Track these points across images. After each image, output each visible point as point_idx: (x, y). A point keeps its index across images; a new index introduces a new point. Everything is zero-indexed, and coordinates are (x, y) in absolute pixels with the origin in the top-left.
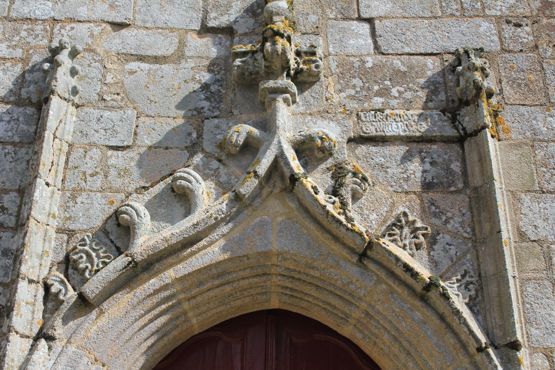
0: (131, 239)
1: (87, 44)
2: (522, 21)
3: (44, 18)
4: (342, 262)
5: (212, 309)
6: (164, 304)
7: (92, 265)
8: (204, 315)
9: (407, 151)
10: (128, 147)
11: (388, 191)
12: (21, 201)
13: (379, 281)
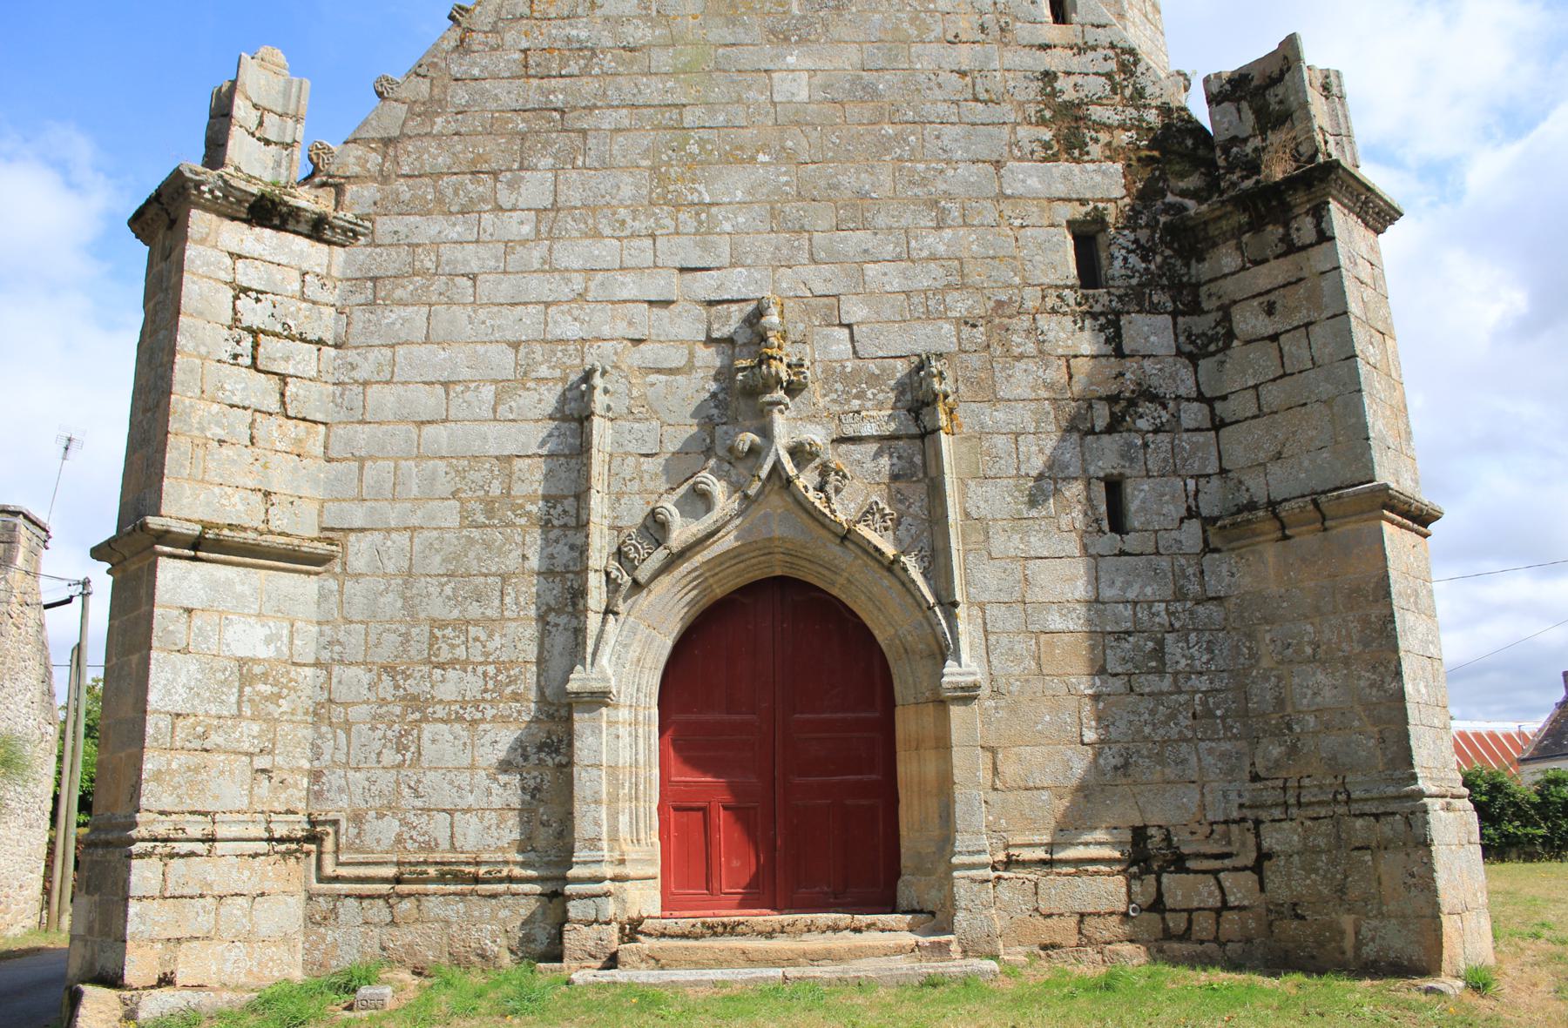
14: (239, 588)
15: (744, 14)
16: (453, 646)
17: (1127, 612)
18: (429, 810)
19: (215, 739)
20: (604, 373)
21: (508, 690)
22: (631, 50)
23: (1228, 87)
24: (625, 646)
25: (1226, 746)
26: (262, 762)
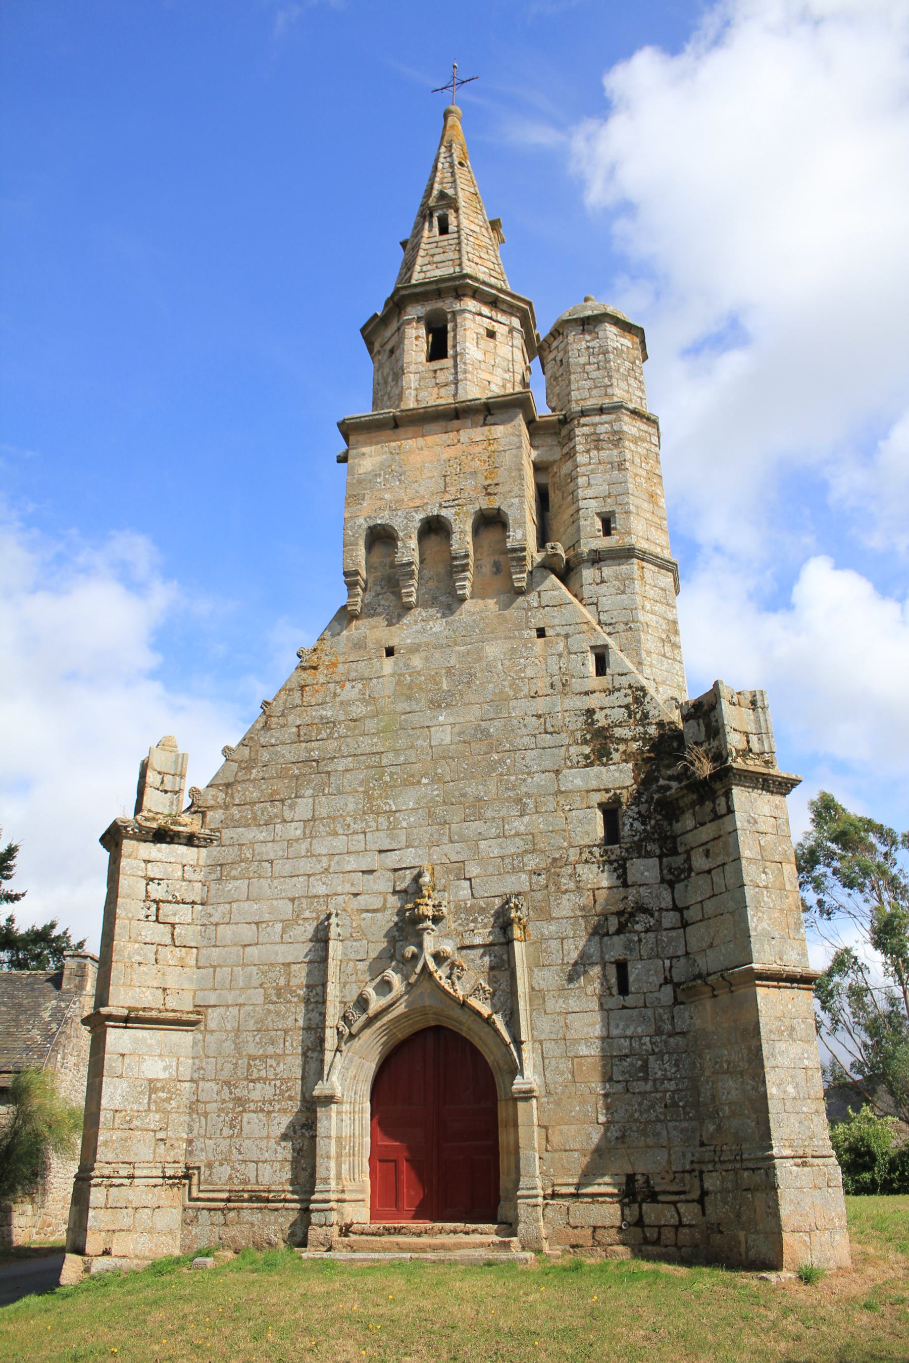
14: (149, 1041)
15: (416, 692)
16: (259, 1070)
17: (626, 1043)
18: (246, 1161)
19: (136, 1123)
20: (337, 915)
21: (287, 1094)
22: (355, 721)
23: (692, 710)
24: (347, 1069)
25: (685, 1124)
26: (160, 1135)
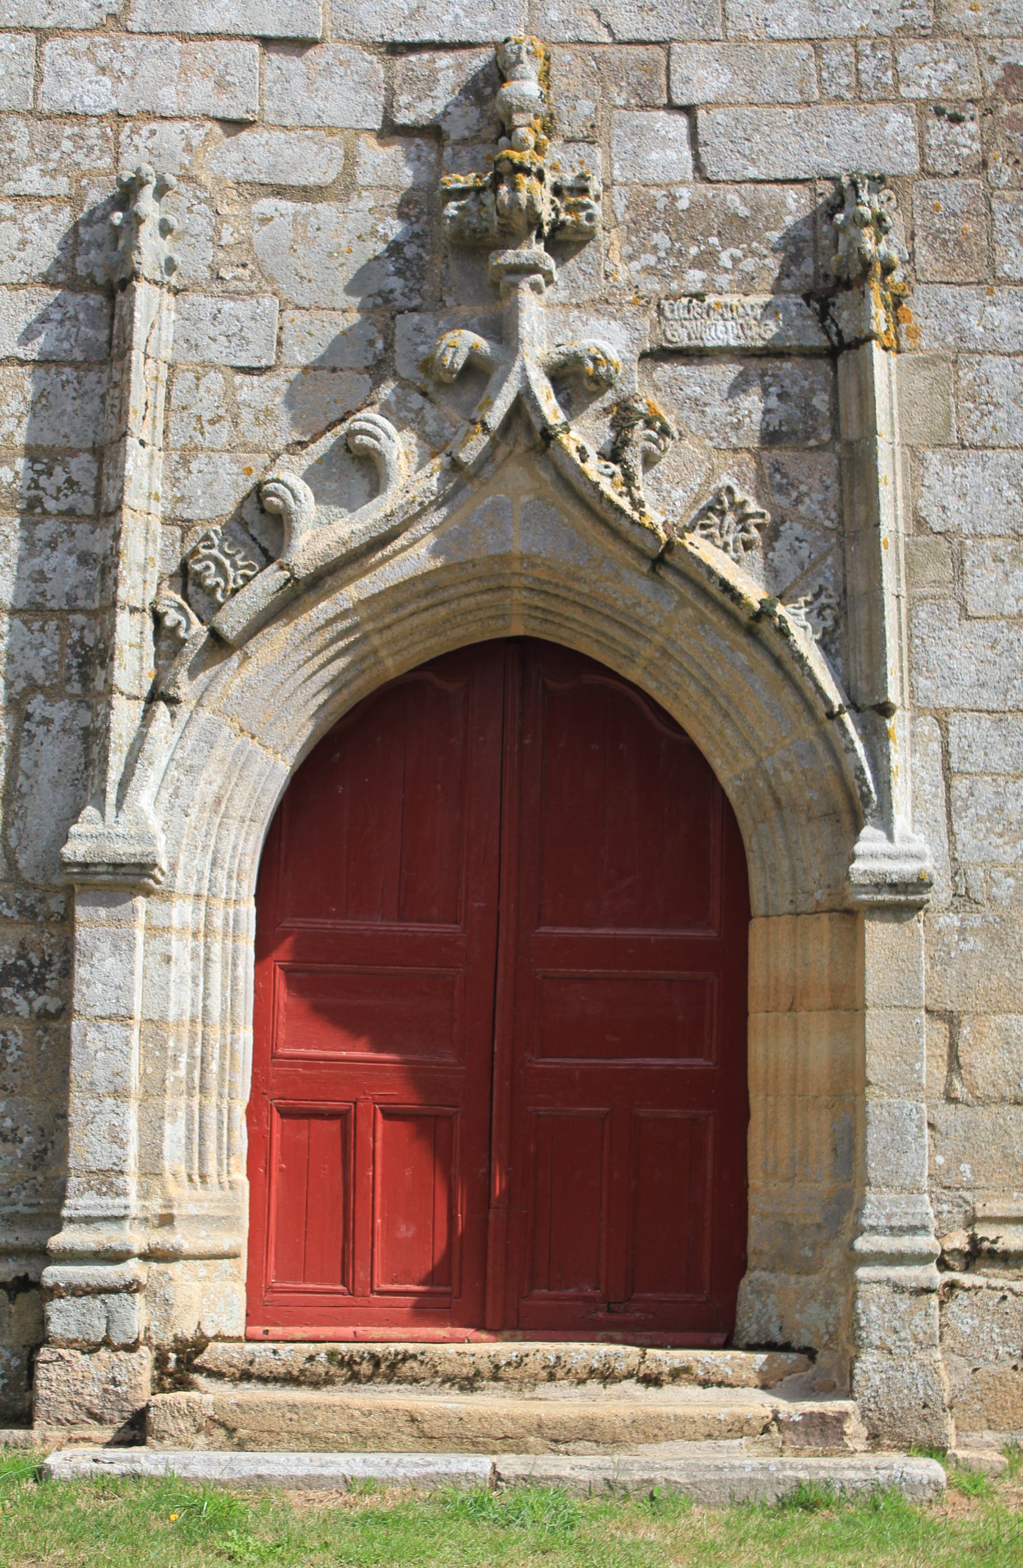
0: (286, 538)
1: (182, 166)
2: (963, 109)
3: (99, 111)
4: (624, 573)
5: (417, 643)
6: (341, 639)
7: (226, 581)
8: (405, 653)
9: (741, 374)
10: (268, 368)
11: (704, 447)
12: (100, 469)
13: (683, 603)
24: (190, 770)
